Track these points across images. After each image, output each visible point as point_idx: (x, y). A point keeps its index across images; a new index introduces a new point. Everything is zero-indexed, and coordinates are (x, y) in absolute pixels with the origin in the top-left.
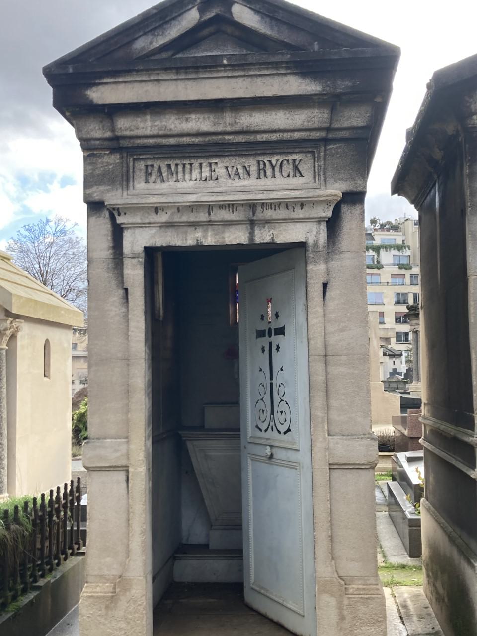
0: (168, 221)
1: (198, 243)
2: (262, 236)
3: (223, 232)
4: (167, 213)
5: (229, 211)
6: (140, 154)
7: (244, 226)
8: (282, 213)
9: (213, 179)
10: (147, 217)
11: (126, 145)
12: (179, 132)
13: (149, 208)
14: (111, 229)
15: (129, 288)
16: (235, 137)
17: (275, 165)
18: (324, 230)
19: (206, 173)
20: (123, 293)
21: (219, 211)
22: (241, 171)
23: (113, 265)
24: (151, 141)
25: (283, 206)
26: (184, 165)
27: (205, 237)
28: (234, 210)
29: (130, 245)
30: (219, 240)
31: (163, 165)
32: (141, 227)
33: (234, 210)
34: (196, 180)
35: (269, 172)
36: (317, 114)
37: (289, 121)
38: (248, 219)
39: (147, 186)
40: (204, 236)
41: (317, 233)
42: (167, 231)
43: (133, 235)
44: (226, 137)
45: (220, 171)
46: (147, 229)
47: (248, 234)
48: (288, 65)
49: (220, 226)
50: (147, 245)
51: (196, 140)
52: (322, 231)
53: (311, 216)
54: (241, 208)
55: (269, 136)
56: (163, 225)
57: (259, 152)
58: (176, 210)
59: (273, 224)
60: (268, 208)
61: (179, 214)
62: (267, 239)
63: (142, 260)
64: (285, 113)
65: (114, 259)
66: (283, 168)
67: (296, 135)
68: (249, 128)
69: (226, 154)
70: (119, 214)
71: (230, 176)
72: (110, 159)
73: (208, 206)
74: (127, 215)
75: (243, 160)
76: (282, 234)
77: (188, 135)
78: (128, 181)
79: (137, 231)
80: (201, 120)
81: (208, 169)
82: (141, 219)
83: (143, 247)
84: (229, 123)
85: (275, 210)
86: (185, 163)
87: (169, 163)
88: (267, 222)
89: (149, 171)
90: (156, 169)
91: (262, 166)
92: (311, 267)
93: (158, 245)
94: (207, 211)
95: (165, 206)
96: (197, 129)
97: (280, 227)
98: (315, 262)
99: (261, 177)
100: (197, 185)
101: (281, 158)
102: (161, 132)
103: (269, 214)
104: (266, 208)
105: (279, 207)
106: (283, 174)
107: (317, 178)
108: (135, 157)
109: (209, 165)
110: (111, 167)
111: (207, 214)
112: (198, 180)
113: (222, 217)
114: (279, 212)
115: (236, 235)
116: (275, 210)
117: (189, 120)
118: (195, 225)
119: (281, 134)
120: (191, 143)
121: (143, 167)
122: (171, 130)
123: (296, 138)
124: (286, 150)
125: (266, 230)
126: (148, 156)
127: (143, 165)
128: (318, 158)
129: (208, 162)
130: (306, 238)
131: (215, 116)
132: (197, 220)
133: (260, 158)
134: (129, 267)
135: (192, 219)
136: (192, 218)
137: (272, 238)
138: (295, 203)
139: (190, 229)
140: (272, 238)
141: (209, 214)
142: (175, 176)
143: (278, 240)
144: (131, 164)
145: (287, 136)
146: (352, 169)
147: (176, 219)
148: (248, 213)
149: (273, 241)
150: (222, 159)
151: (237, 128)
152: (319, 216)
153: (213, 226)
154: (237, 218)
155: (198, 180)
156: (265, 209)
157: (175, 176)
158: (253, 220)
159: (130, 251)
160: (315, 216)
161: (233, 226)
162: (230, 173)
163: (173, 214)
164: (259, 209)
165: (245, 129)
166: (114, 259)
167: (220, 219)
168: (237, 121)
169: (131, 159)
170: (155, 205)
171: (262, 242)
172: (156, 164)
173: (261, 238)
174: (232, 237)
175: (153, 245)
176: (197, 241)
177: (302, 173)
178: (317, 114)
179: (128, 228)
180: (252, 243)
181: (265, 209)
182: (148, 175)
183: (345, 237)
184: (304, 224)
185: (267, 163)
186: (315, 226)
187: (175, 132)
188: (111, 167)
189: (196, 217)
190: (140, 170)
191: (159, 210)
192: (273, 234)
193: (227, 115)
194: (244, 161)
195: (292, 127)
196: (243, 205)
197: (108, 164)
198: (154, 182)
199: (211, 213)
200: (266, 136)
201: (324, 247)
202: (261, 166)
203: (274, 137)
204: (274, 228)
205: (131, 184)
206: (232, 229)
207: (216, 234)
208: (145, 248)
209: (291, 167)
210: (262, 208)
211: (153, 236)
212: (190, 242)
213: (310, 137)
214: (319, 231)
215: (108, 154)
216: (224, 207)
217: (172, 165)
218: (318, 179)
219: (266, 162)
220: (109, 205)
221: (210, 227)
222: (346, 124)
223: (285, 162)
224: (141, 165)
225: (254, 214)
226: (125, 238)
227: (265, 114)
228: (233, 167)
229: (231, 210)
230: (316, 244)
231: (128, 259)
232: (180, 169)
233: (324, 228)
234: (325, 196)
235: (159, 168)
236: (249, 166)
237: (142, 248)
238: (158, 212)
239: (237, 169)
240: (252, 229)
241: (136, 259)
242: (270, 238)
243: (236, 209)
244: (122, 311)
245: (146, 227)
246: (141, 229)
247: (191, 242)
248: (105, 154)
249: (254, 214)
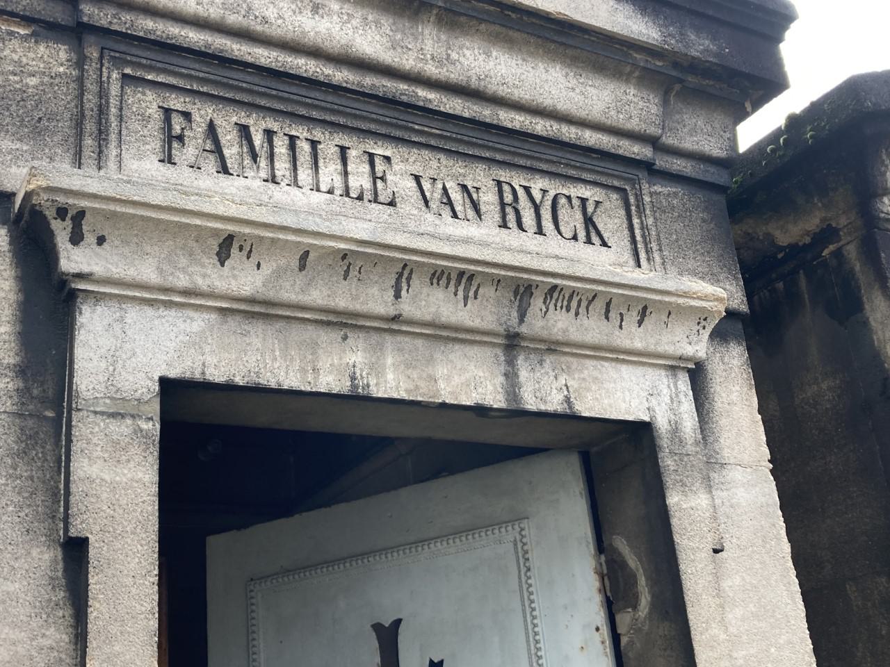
0: (260, 297)
1: (354, 386)
2: (539, 390)
3: (430, 361)
4: (259, 266)
5: (456, 294)
6: (151, 69)
7: (488, 352)
8: (591, 328)
9: (381, 198)
10: (184, 270)
11: (104, 23)
12: (290, 36)
13: (200, 234)
14: (12, 297)
15: (92, 539)
16: (444, 100)
17: (541, 202)
18: (686, 395)
19: (360, 179)
20: (55, 561)
21: (425, 290)
22: (456, 196)
23: (11, 439)
24: (194, 37)
25: (599, 305)
26: (293, 139)
27: (376, 368)
28: (471, 294)
29: (103, 365)
30: (422, 384)
31: (227, 121)
32: (150, 303)
33: (471, 294)
34: (330, 192)
35: (528, 218)
36: (636, 100)
37: (578, 98)
38: (507, 330)
39: (165, 171)
40: (372, 367)
41: (672, 402)
42: (245, 334)
43: (117, 327)
44: (422, 93)
45: (399, 181)
46: (173, 312)
47: (501, 379)
48: (23, 222)
49: (419, 342)
50: (173, 374)
51: (341, 76)
52: (682, 396)
53: (660, 349)
54: (487, 291)
55: (527, 122)
56: (235, 306)
57: (499, 157)
58: (295, 263)
59: (563, 359)
60: (559, 305)
61: (301, 279)
62: (554, 403)
63: (153, 427)
64: (567, 75)
65: (19, 415)
66: (560, 217)
67: (590, 138)
68: (482, 83)
69: (416, 139)
70: (76, 238)
71: (426, 202)
72: (31, 55)
73: (398, 268)
74: (105, 245)
75: (459, 167)
76: (588, 390)
77: (315, 53)
78: (102, 136)
79: (134, 314)
80: (355, 22)
81: (366, 168)
82: (160, 271)
83: (157, 378)
84: (432, 55)
85: (577, 314)
86: (293, 133)
87: (243, 121)
88: (552, 347)
89: (177, 129)
90: (199, 128)
91: (508, 198)
92: (676, 499)
93: (217, 375)
94: (393, 282)
95: (261, 239)
96: (343, 42)
97: (581, 371)
98: (684, 485)
99: (510, 225)
100: (335, 208)
101: (554, 187)
102: (233, 19)
103: (560, 325)
104: (556, 306)
105: (587, 308)
106: (562, 229)
107: (643, 255)
108: (128, 71)
109: (366, 157)
110: (33, 81)
111: (391, 293)
112: (338, 192)
113: (433, 309)
114: (586, 322)
115: (467, 375)
116: (577, 314)
117: (321, 11)
118: (345, 325)
119: (556, 126)
120: (322, 78)
121: (153, 111)
122: (265, 21)
123: (590, 144)
124: (561, 170)
125: (547, 373)
126: (172, 80)
127: (155, 106)
128: (638, 206)
129: (362, 147)
130: (648, 409)
131: (394, 24)
132: (357, 307)
133: (504, 175)
134: (98, 452)
135: (342, 303)
136: (342, 297)
137: (567, 400)
138: (629, 302)
139: (326, 337)
140: (567, 400)
141: (397, 296)
142: (263, 163)
143: (586, 408)
144: (114, 90)
145: (569, 133)
146: (708, 252)
147: (290, 292)
148: (506, 310)
149: (570, 408)
150: (404, 150)
151: (453, 74)
152: (679, 353)
153: (399, 338)
154: (476, 323)
155: (338, 192)
156: (552, 307)
157: (263, 163)
158: (517, 335)
159: (101, 388)
160: (671, 350)
161: (457, 347)
162: (428, 194)
163: (279, 274)
164: (537, 303)
165: (474, 83)
166: (19, 415)
167: (428, 318)
168: (454, 56)
169: (115, 75)
170: (231, 228)
171: (543, 408)
172: (203, 113)
173: (538, 394)
174: (456, 380)
175: (198, 376)
176: (353, 378)
177: (606, 235)
178: (636, 100)
179: (98, 297)
180: (514, 406)
181: (552, 307)
182: (171, 140)
183: (723, 422)
184: (640, 370)
185: (521, 192)
186: (665, 380)
187: (275, 31)
188: (33, 81)
189: (355, 298)
190: (146, 119)
191: (234, 251)
192: (566, 385)
193: (427, 32)
194: (462, 171)
195: (583, 114)
196: (498, 281)
197: (21, 70)
198: (194, 166)
199: (404, 293)
200: (522, 119)
201: (697, 443)
202: (505, 195)
203: (541, 126)
204: (568, 370)
205: (113, 151)
206: (457, 354)
207: (408, 366)
208: (164, 381)
209: (579, 215)
210: (545, 302)
211: (196, 343)
212: (329, 381)
213: (621, 152)
214: (677, 396)
215: (25, 38)
216: (443, 281)
217: (252, 129)
218: (648, 259)
219: (517, 187)
220: (49, 189)
221: (388, 338)
222: (688, 144)
223: (563, 201)
224: (149, 103)
225: (521, 320)
226: (81, 337)
227: (520, 62)
228: (435, 180)
229: (461, 293)
230: (675, 430)
231: (92, 418)
232: (281, 147)
233: (685, 389)
234: (699, 298)
235: (211, 129)
236: (478, 189)
237: (151, 379)
238: (228, 256)
239: (444, 188)
240: (511, 362)
241: (129, 421)
242: (560, 397)
243: (476, 293)
244: (47, 642)
245: (169, 304)
246: (149, 311)
247: (330, 378)
248: (11, 33)
249: (521, 320)
